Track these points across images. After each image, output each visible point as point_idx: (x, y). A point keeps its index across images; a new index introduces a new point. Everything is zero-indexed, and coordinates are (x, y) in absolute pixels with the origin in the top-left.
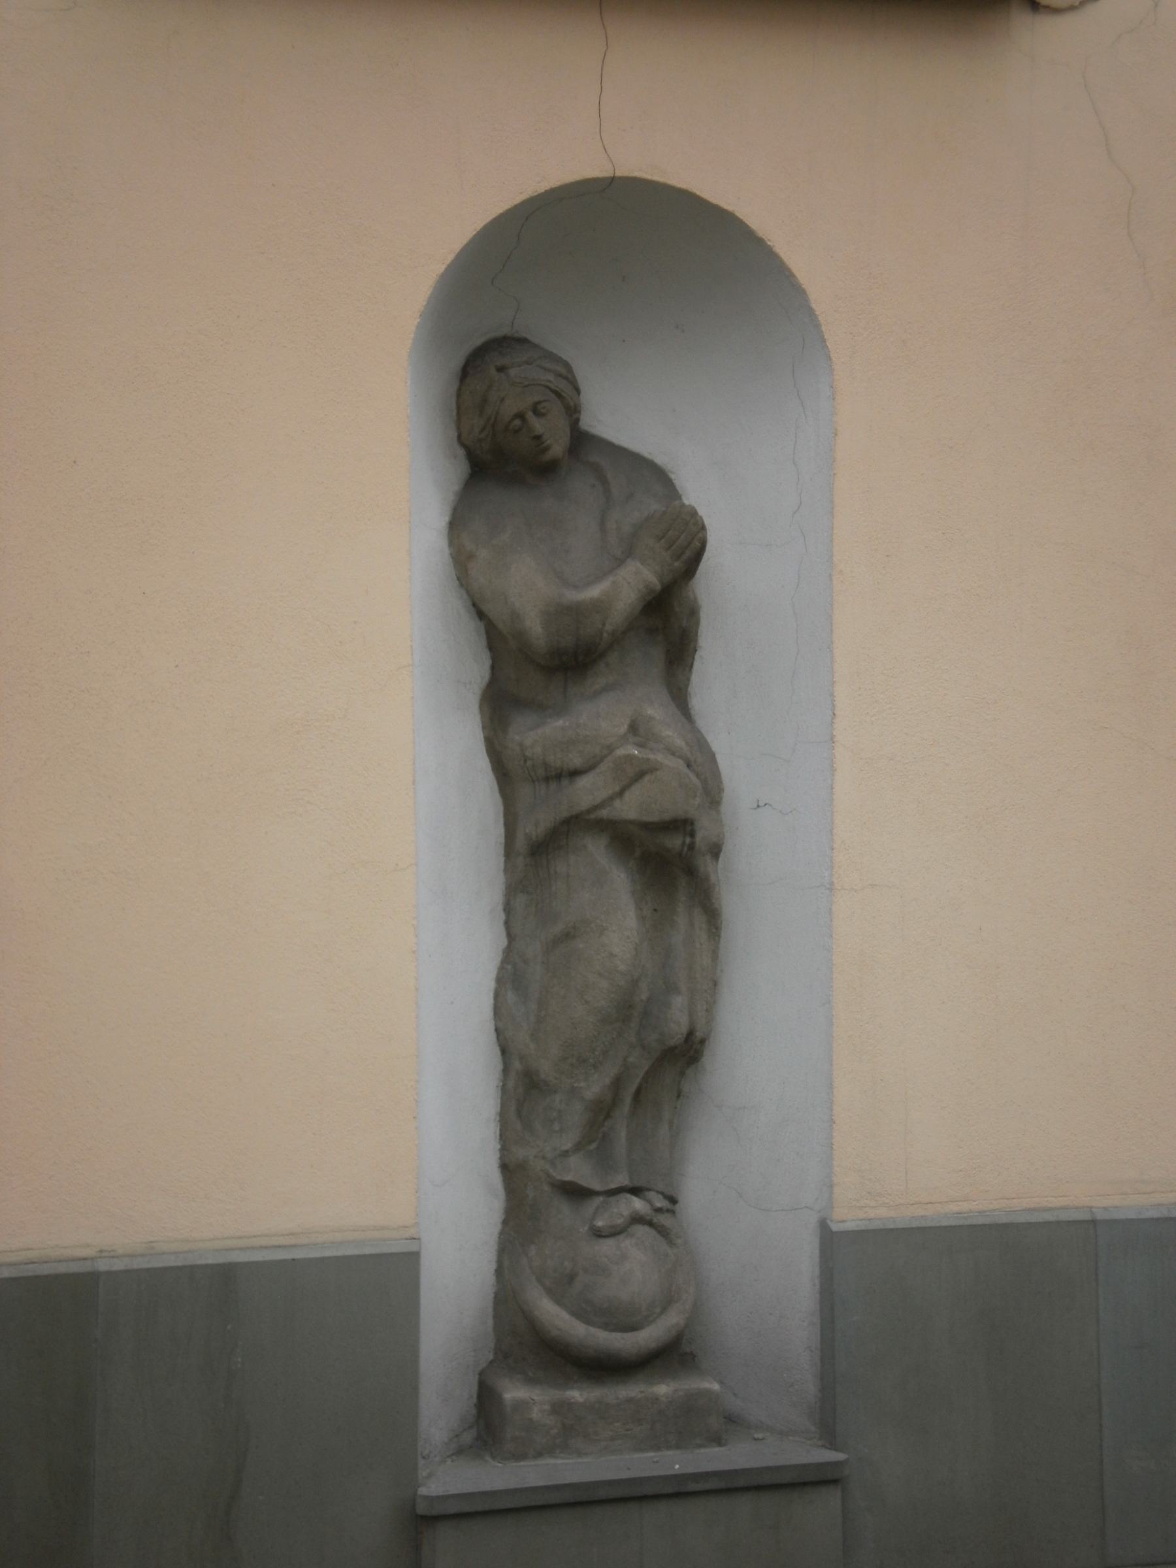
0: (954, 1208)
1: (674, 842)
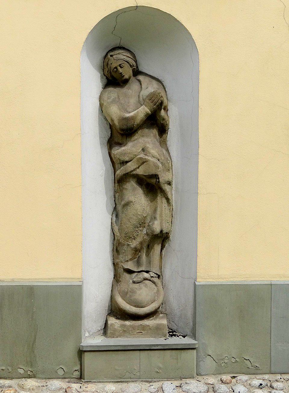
0: (283, 279)
1: (153, 181)
